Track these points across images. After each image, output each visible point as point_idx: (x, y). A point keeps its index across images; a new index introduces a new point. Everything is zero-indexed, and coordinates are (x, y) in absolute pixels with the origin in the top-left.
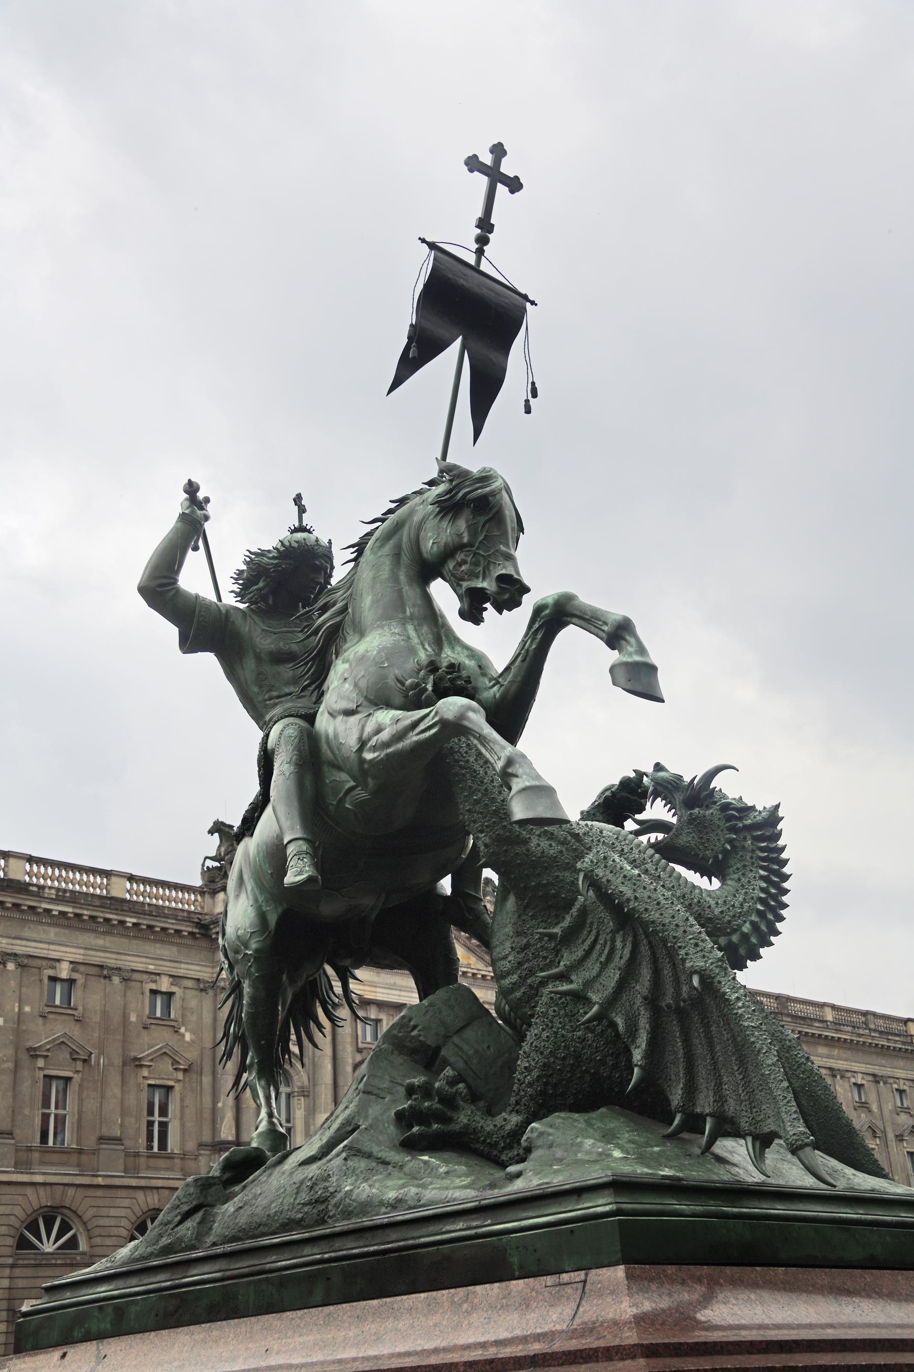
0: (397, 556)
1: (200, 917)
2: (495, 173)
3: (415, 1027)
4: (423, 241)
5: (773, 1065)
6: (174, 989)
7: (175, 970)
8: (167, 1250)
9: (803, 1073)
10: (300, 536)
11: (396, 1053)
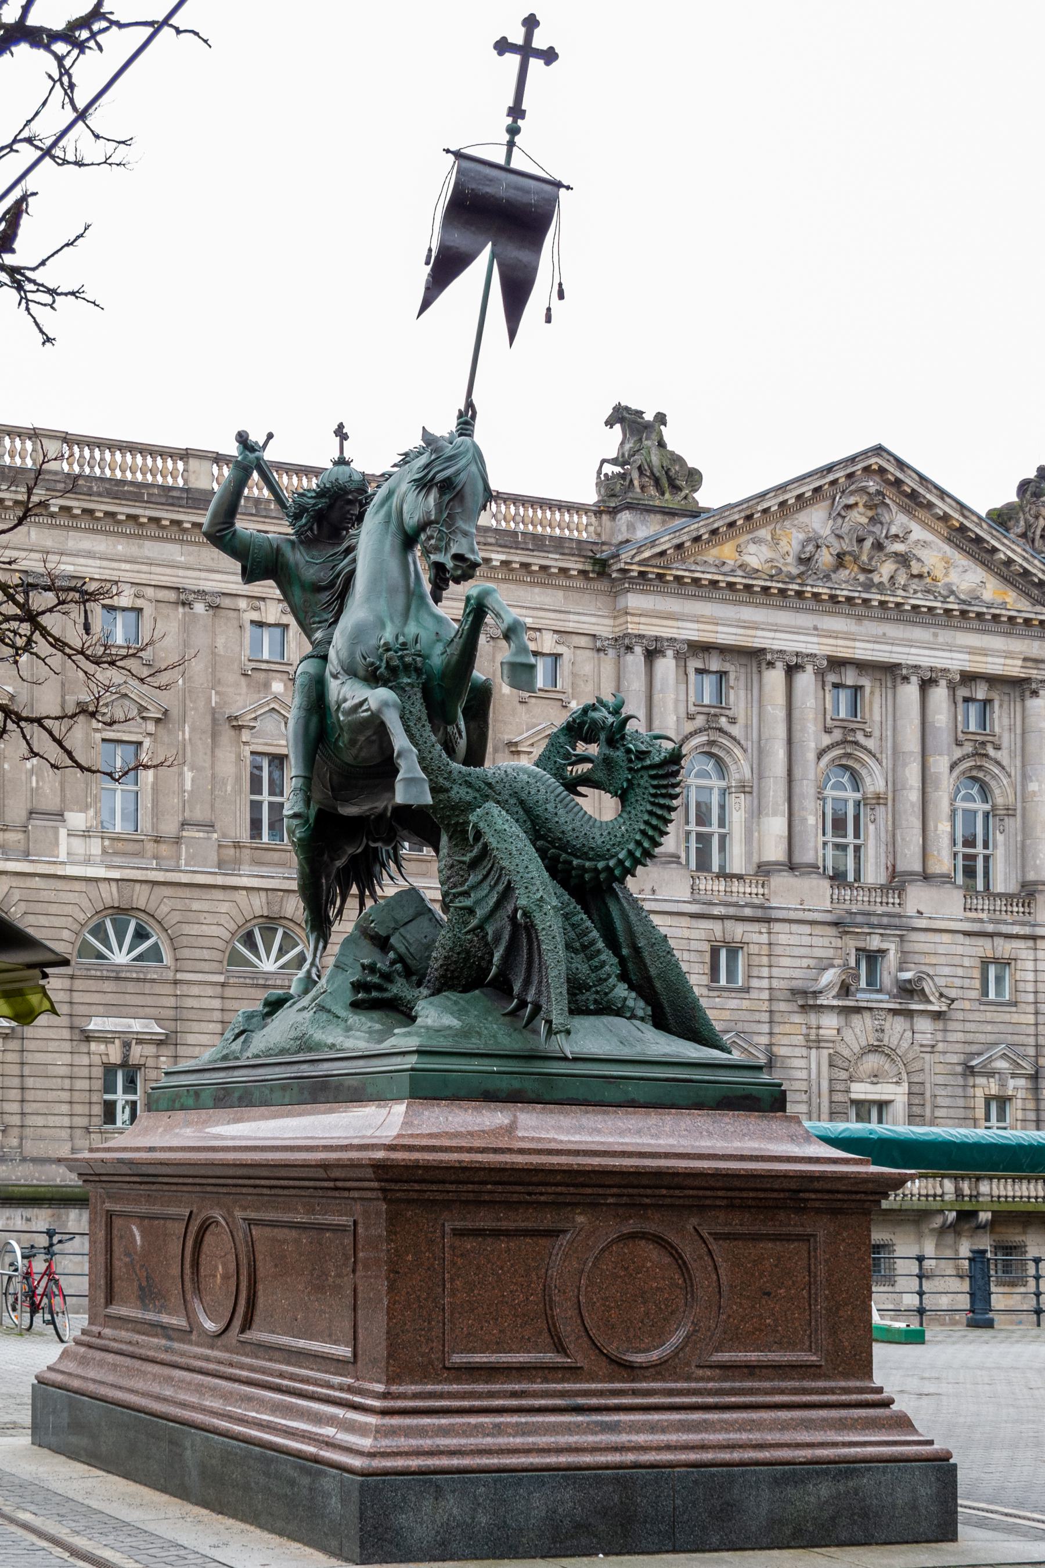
0: (387, 522)
1: (594, 548)
2: (526, 50)
4: (448, 151)
6: (560, 649)
8: (225, 1058)
10: (342, 468)
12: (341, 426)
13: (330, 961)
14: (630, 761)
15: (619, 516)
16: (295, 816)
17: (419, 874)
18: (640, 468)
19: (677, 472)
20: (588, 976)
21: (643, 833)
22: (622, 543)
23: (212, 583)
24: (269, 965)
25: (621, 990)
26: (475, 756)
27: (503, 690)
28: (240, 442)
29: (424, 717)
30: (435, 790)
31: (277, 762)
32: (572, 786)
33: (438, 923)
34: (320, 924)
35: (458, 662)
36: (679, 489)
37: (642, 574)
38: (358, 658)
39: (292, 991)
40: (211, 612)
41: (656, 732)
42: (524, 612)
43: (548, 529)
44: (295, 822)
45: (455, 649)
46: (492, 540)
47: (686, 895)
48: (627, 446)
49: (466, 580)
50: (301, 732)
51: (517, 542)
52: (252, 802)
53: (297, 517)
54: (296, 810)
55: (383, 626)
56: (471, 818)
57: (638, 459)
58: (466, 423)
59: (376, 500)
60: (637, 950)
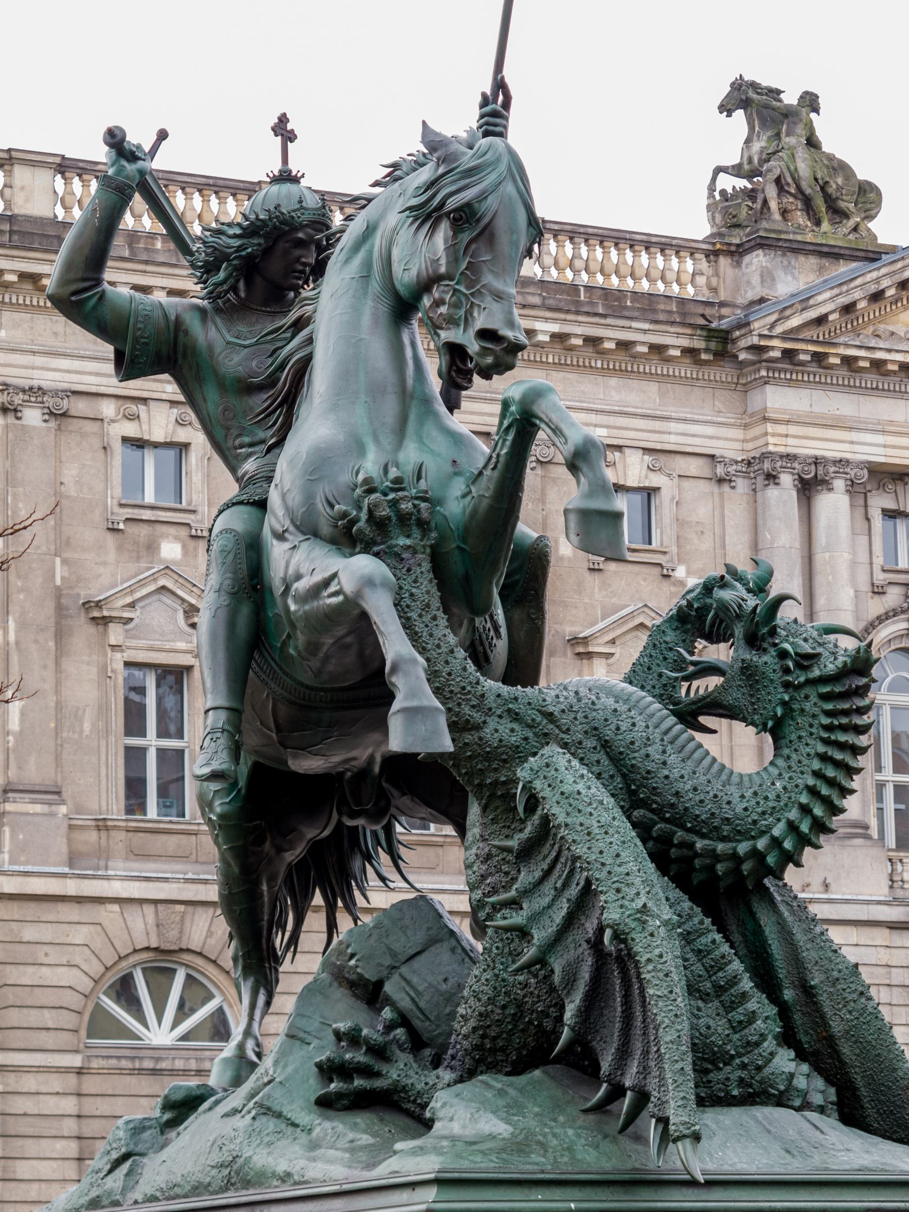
0: (366, 277)
1: (708, 311)
3: (352, 956)
5: (672, 1042)
6: (655, 480)
7: (656, 437)
9: (850, 1012)
10: (286, 188)
11: (336, 984)
12: (283, 120)
13: (276, 1025)
14: (787, 671)
15: (747, 259)
16: (215, 776)
17: (431, 869)
18: (778, 181)
19: (839, 188)
20: (728, 1039)
21: (813, 791)
22: (752, 303)
23: (53, 374)
24: (160, 1034)
25: (784, 1062)
26: (523, 667)
27: (564, 550)
28: (111, 145)
29: (436, 603)
30: (457, 727)
31: (171, 679)
32: (690, 715)
33: (468, 955)
34: (259, 962)
35: (491, 508)
36: (845, 215)
37: (789, 354)
38: (320, 505)
39: (213, 1081)
40: (53, 424)
41: (824, 620)
42: (593, 418)
43: (630, 281)
44: (214, 786)
45: (486, 487)
46: (536, 300)
47: (883, 892)
48: (756, 146)
49: (500, 373)
50: (222, 632)
51: (578, 303)
52: (128, 749)
53: (208, 269)
54: (216, 765)
55: (361, 450)
56: (520, 773)
57: (775, 166)
58: (495, 114)
59: (346, 240)
60: (807, 991)
